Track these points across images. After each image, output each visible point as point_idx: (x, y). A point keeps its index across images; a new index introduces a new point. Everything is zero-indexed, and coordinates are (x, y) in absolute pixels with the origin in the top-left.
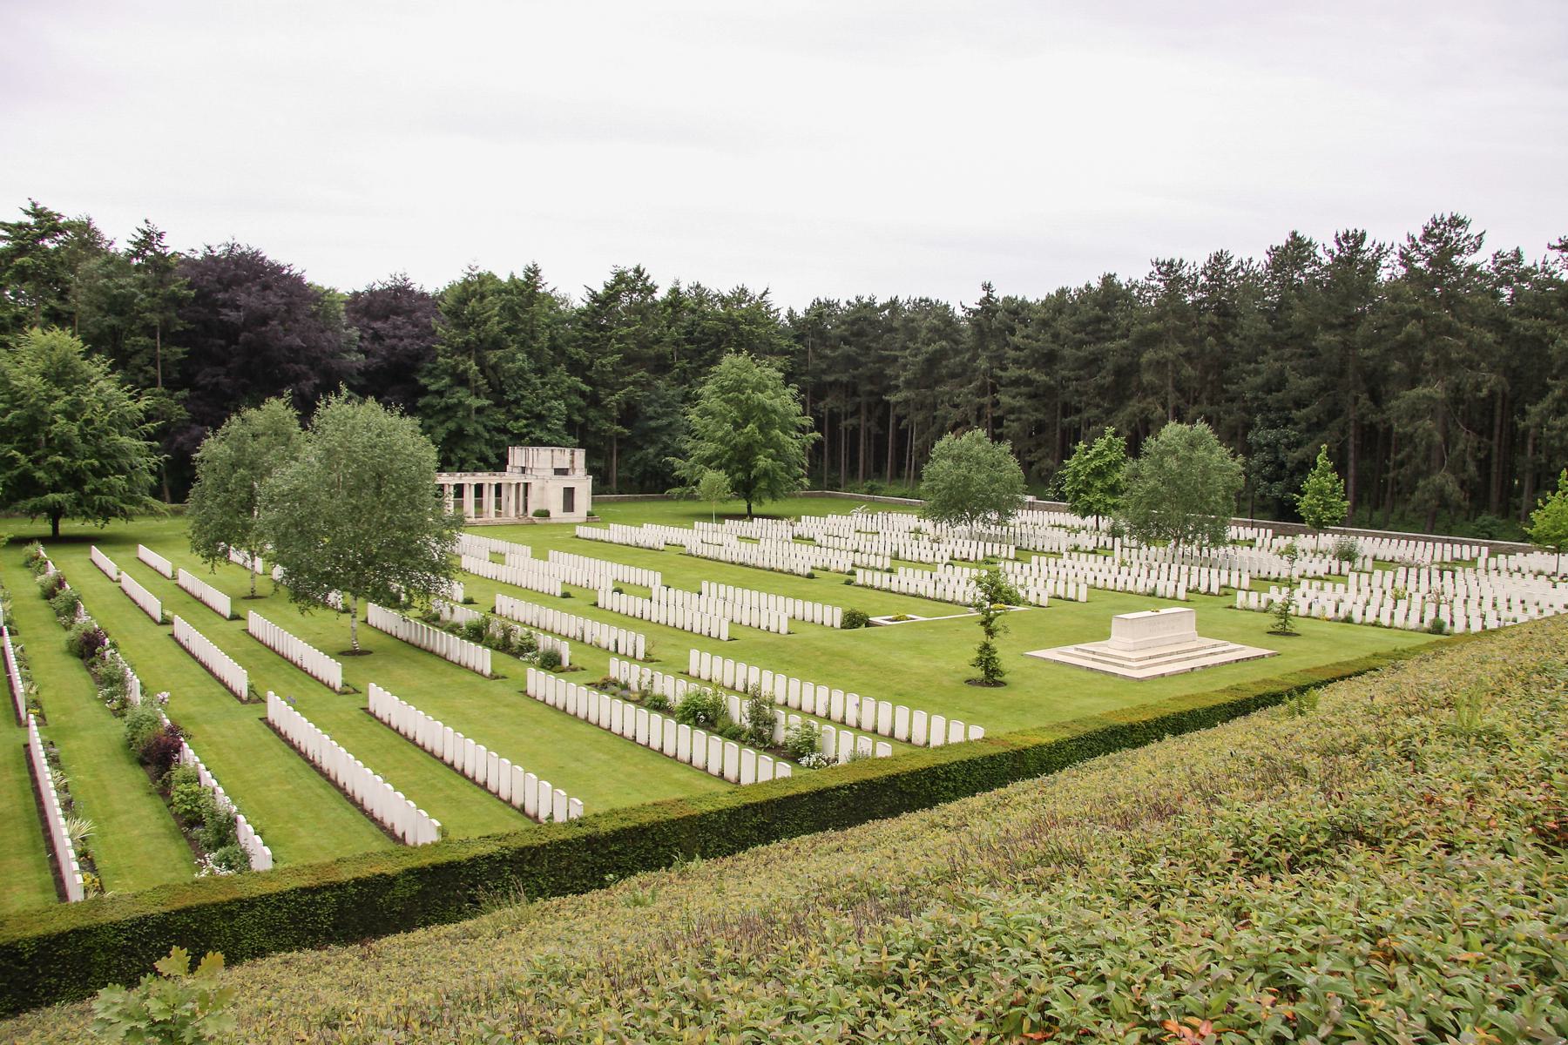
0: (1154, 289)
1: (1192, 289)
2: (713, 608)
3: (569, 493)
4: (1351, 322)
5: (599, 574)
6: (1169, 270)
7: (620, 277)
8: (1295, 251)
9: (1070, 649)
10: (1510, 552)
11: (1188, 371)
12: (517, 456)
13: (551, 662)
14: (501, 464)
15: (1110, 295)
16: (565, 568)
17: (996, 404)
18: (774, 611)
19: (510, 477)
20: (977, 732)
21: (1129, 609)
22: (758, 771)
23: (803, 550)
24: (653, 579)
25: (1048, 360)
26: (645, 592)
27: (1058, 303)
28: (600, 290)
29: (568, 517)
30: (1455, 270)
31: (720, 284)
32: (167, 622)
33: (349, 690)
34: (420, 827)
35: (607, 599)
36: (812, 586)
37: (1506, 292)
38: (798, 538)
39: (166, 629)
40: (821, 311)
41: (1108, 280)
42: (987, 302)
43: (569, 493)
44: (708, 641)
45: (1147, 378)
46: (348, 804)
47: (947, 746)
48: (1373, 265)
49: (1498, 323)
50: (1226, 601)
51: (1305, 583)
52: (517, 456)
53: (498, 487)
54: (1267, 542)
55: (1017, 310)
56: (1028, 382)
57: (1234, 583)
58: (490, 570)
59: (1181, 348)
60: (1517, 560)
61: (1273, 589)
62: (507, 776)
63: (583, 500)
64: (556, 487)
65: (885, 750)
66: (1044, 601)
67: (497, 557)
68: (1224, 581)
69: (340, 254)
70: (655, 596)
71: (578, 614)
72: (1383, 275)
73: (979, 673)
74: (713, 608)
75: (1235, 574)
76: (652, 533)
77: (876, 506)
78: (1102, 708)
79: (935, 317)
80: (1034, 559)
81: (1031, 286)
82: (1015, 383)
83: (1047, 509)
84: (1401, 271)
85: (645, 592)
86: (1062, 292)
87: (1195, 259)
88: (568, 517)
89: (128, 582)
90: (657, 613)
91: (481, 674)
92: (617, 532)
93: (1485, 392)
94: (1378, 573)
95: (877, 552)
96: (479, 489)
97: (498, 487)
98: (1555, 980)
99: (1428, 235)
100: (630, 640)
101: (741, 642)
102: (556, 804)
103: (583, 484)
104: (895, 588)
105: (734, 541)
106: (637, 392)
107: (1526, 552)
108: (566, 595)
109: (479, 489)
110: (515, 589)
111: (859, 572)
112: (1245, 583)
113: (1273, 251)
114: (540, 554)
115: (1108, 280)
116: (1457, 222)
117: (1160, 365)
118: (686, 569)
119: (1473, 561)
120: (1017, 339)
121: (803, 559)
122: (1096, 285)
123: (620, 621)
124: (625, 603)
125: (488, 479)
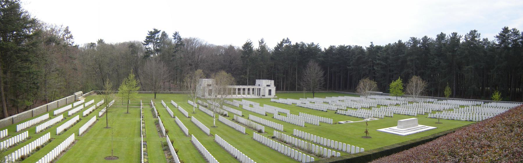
0: (411, 44)
1: (419, 43)
2: (301, 119)
3: (270, 91)
4: (454, 51)
5: (274, 110)
6: (414, 39)
7: (284, 40)
8: (441, 37)
9: (388, 129)
10: (488, 102)
12: (258, 82)
13: (260, 132)
14: (254, 84)
15: (400, 45)
16: (267, 108)
17: (374, 69)
18: (316, 120)
19: (256, 87)
20: (363, 149)
23: (388, 101)
24: (288, 111)
25: (386, 59)
26: (285, 114)
27: (389, 47)
28: (280, 43)
29: (269, 97)
30: (476, 41)
31: (307, 42)
32: (174, 117)
33: (212, 135)
35: (276, 116)
36: (327, 114)
37: (486, 46)
38: (324, 102)
40: (332, 48)
41: (400, 41)
42: (371, 46)
43: (270, 91)
44: (299, 127)
45: (408, 63)
48: (459, 40)
49: (485, 52)
50: (426, 116)
52: (258, 82)
55: (379, 48)
56: (381, 64)
58: (249, 108)
59: (416, 57)
60: (489, 104)
61: (437, 113)
64: (268, 89)
65: (339, 154)
66: (383, 117)
67: (251, 106)
70: (288, 115)
71: (270, 120)
72: (461, 41)
73: (365, 135)
74: (301, 119)
76: (289, 101)
78: (394, 143)
79: (359, 49)
81: (392, 43)
82: (378, 64)
83: (386, 95)
84: (465, 41)
85: (285, 114)
86: (389, 44)
87: (420, 37)
88: (269, 97)
89: (168, 108)
90: (286, 119)
91: (242, 133)
92: (281, 100)
93: (482, 67)
94: (460, 108)
95: (343, 106)
96: (249, 89)
97: (253, 89)
99: (470, 34)
100: (281, 127)
101: (308, 127)
103: (273, 89)
104: (347, 114)
105: (309, 103)
107: (491, 102)
108: (266, 115)
109: (249, 89)
110: (254, 113)
112: (431, 111)
113: (438, 36)
114: (261, 105)
115: (400, 41)
116: (475, 31)
117: (412, 60)
118: (296, 109)
119: (480, 105)
120: (379, 54)
121: (325, 107)
122: (397, 42)
125: (251, 87)
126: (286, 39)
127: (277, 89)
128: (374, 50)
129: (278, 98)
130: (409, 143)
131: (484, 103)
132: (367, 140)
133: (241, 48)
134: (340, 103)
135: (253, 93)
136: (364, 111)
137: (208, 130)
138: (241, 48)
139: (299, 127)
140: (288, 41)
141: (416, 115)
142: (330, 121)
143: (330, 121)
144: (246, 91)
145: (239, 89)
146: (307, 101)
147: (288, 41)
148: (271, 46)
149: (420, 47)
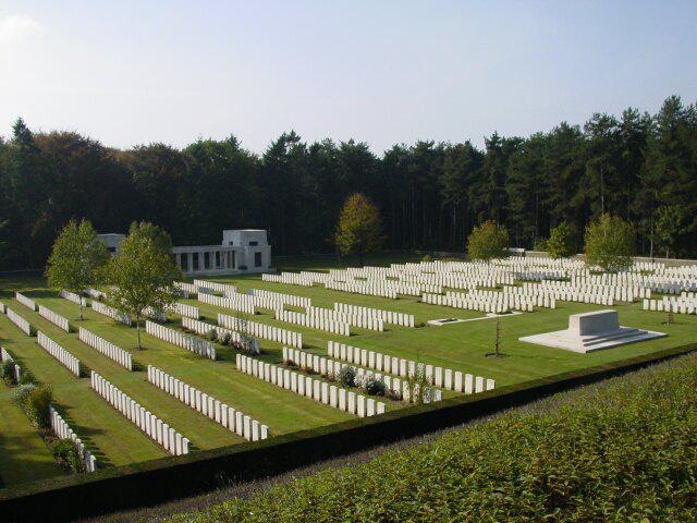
2: (339, 319)
3: (258, 256)
11: (611, 168)
14: (219, 241)
15: (566, 135)
18: (375, 319)
20: (491, 385)
21: (550, 299)
22: (372, 408)
23: (391, 284)
24: (306, 302)
26: (302, 310)
28: (276, 141)
34: (178, 446)
35: (281, 315)
39: (33, 339)
41: (564, 126)
44: (338, 338)
46: (653, 358)
47: (485, 392)
51: (684, 294)
53: (218, 253)
54: (662, 272)
55: (513, 144)
57: (642, 296)
62: (225, 414)
63: (266, 259)
68: (636, 295)
69: (121, 129)
74: (339, 319)
75: (642, 290)
76: (306, 278)
77: (432, 260)
79: (466, 151)
80: (525, 284)
85: (302, 310)
98: (593, 206)
100: (297, 339)
101: (357, 337)
102: (253, 430)
106: (315, 205)
108: (258, 313)
111: (424, 295)
112: (649, 294)
121: (391, 290)
123: (334, 332)
124: (291, 317)
125: (213, 249)
126: (289, 133)
127: (274, 253)
128: (503, 150)
129: (278, 273)
130: (158, 467)
131: (667, 267)
132: (500, 361)
133: (261, 157)
134: (424, 278)
135: (218, 264)
136: (483, 295)
137: (126, 360)
138: (261, 157)
139: (338, 338)
140: (293, 138)
141: (611, 303)
142: (408, 320)
143: (408, 320)
144: (201, 260)
145: (184, 256)
146: (336, 278)
147: (293, 138)
148: (379, 151)
149: (617, 133)
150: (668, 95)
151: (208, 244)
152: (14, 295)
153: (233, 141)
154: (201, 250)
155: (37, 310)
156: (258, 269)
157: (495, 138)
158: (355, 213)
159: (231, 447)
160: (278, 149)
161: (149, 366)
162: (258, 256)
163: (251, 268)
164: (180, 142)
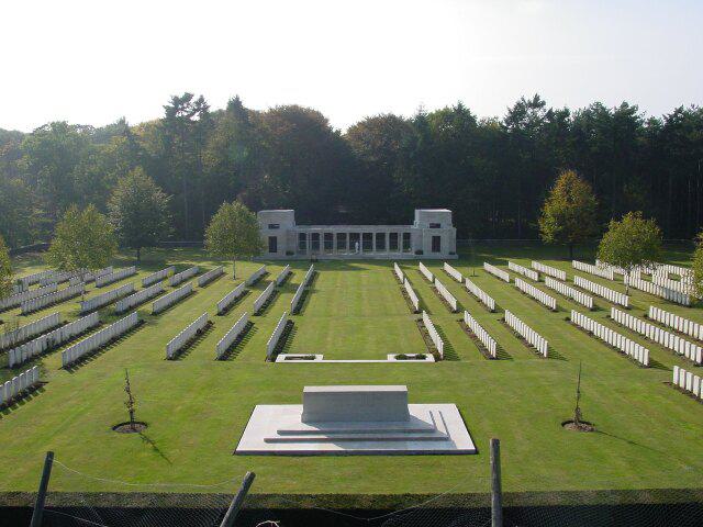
3: (436, 242)
14: (409, 220)
125: (400, 229)
127: (461, 235)
133: (344, 132)
138: (344, 132)
140: (537, 103)
145: (315, 236)
150: (232, 96)
151: (395, 224)
152: (506, 263)
153: (122, 122)
154: (387, 230)
155: (464, 282)
156: (437, 255)
157: (633, 110)
158: (564, 195)
159: (132, 495)
160: (518, 113)
161: (676, 368)
162: (436, 242)
163: (428, 253)
164: (407, 112)
